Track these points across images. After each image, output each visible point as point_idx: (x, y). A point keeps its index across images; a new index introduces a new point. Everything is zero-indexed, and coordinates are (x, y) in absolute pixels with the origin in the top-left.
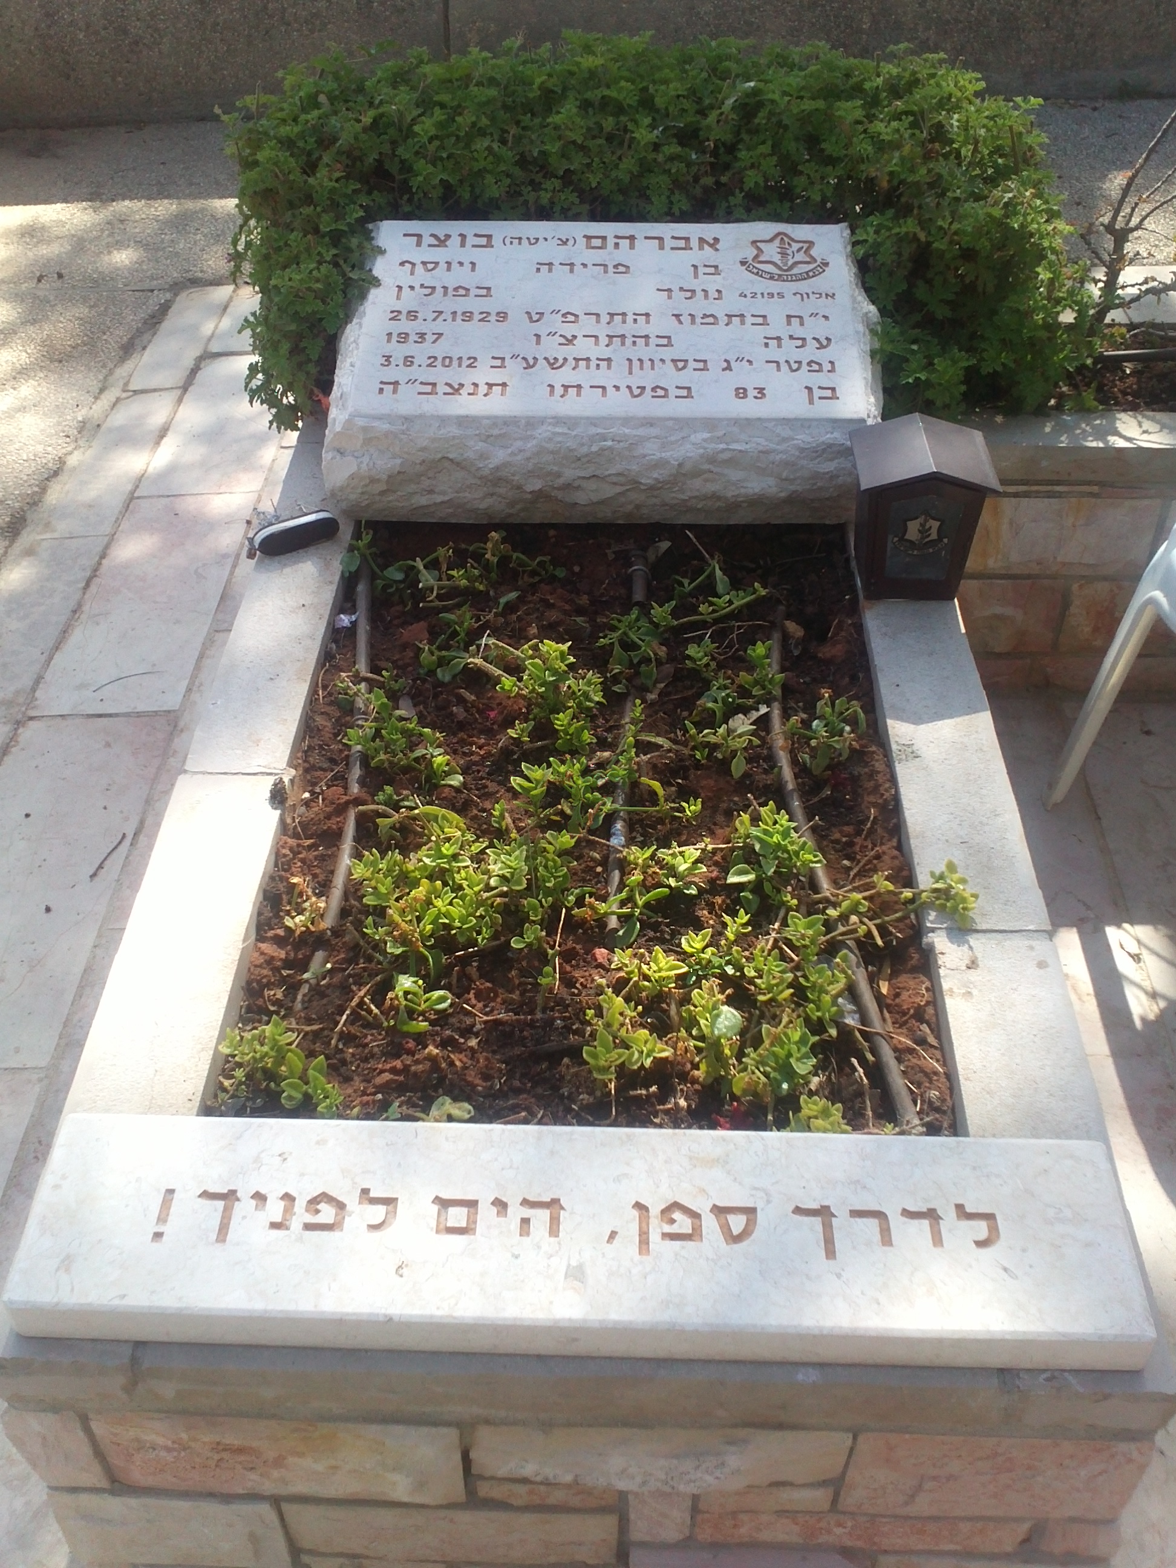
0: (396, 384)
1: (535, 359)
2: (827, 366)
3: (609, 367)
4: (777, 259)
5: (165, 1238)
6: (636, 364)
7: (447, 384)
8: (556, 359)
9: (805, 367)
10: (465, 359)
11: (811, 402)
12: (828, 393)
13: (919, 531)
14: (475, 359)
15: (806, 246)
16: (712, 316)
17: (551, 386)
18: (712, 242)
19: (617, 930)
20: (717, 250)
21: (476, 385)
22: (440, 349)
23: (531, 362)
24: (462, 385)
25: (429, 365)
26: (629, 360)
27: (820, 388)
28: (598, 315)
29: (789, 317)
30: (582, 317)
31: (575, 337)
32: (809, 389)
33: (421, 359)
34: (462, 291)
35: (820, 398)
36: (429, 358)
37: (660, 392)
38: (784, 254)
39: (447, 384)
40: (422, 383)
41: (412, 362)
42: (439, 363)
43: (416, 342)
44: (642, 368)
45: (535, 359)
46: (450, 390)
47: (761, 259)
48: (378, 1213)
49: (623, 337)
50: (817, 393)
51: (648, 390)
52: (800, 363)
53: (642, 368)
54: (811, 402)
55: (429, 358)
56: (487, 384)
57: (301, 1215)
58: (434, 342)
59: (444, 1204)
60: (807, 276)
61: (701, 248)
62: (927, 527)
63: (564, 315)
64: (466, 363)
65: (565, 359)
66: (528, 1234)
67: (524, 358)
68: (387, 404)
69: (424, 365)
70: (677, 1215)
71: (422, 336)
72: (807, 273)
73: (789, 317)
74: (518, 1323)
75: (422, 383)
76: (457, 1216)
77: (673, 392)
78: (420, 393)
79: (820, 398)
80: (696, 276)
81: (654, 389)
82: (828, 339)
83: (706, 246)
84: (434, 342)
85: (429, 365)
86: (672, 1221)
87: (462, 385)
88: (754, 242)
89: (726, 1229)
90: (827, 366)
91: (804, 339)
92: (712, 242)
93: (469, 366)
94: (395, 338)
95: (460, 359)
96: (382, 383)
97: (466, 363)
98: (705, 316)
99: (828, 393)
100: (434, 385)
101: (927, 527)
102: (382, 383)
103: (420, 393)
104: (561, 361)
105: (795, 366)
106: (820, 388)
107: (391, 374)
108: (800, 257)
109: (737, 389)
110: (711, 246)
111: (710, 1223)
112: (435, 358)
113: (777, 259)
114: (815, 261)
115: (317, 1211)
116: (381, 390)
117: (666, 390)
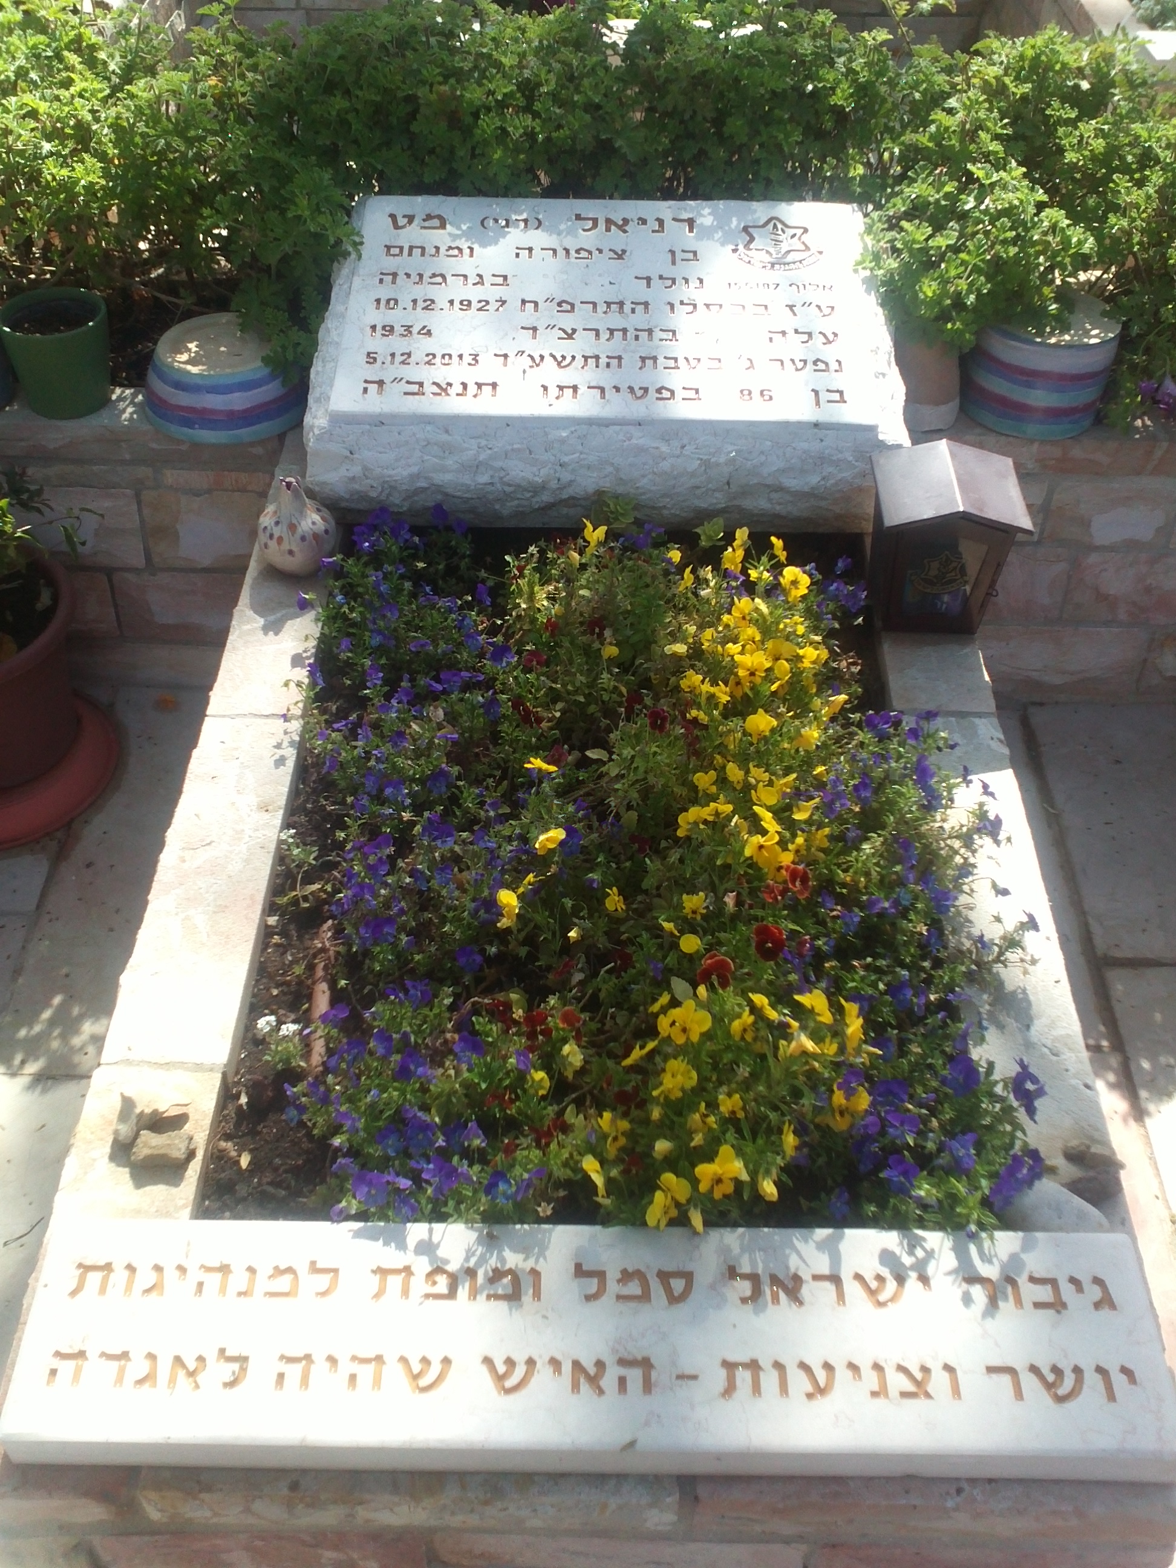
0: (381, 383)
3: (620, 366)
8: (510, 1363)
9: (810, 366)
12: (837, 397)
15: (799, 232)
18: (620, 223)
23: (538, 360)
25: (429, 363)
28: (595, 304)
30: (578, 305)
37: (821, 366)
40: (408, 382)
41: (375, 359)
46: (437, 390)
48: (324, 1280)
49: (625, 331)
50: (824, 396)
52: (805, 362)
57: (263, 1284)
61: (608, 230)
63: (559, 304)
65: (573, 357)
66: (993, 1317)
68: (374, 404)
71: (408, 329)
73: (524, 302)
75: (408, 382)
77: (429, 388)
78: (406, 394)
80: (674, 263)
81: (815, 363)
82: (836, 335)
83: (613, 227)
87: (450, 385)
89: (668, 1290)
90: (834, 366)
91: (810, 334)
93: (403, 363)
96: (366, 381)
97: (399, 359)
99: (837, 397)
100: (421, 384)
102: (366, 381)
103: (406, 394)
104: (568, 359)
107: (373, 373)
110: (620, 227)
111: (655, 1286)
112: (434, 356)
114: (807, 248)
115: (435, 1283)
116: (365, 390)
117: (827, 364)
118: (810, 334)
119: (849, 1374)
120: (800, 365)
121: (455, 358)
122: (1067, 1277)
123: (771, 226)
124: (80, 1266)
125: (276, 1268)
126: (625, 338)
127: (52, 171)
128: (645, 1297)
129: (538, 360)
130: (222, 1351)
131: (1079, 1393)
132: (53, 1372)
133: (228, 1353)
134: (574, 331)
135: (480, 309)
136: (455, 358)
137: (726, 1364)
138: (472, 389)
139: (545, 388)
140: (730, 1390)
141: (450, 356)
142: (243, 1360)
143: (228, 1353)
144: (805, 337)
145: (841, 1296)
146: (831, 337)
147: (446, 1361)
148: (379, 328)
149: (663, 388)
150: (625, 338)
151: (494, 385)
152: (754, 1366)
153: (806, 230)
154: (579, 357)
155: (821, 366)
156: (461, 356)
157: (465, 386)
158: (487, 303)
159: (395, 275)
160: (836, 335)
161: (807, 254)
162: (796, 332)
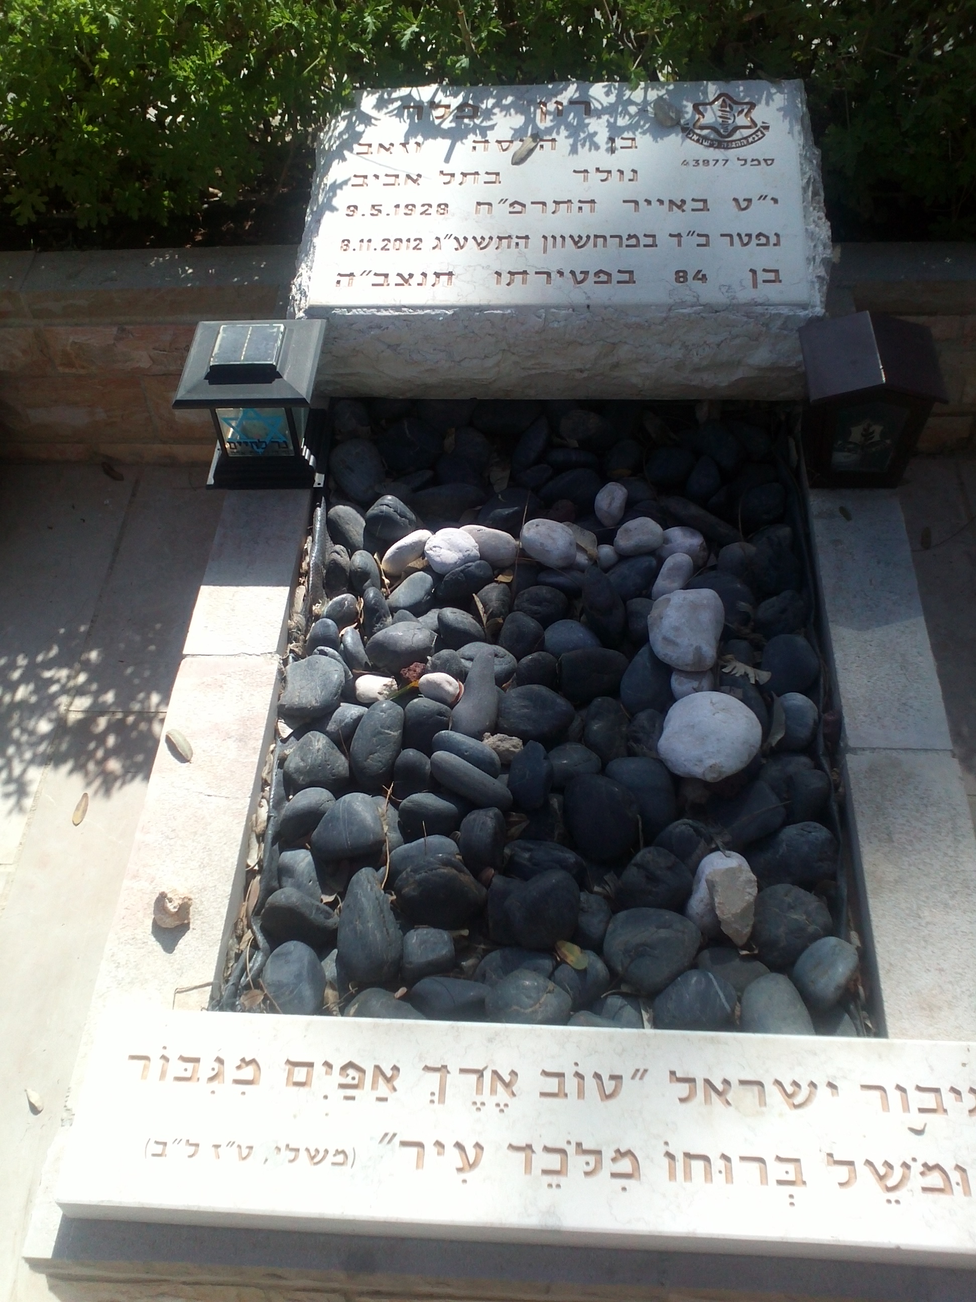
1: (466, 239)
2: (773, 240)
6: (559, 240)
7: (399, 275)
8: (580, 237)
10: (412, 240)
11: (755, 285)
13: (863, 435)
14: (420, 240)
16: (757, 160)
18: (679, 203)
19: (27, 101)
20: (683, 211)
24: (411, 276)
25: (382, 249)
26: (545, 237)
27: (764, 270)
29: (479, 204)
32: (753, 272)
35: (764, 281)
36: (384, 240)
37: (603, 278)
39: (399, 275)
40: (376, 274)
44: (554, 245)
45: (466, 239)
50: (762, 276)
51: (591, 275)
53: (554, 245)
54: (755, 285)
55: (384, 240)
57: (230, 1072)
58: (714, 165)
60: (746, 141)
62: (871, 430)
63: (512, 205)
64: (413, 244)
65: (491, 238)
67: (456, 238)
69: (379, 249)
72: (746, 138)
74: (690, 1235)
75: (376, 274)
77: (616, 277)
79: (764, 281)
81: (597, 274)
83: (674, 207)
84: (714, 165)
87: (411, 276)
90: (773, 240)
92: (679, 203)
95: (408, 240)
98: (753, 160)
100: (386, 276)
101: (871, 430)
102: (340, 275)
104: (584, 239)
109: (677, 272)
110: (679, 207)
117: (767, 238)
120: (580, 277)
122: (914, 1087)
124: (288, 1062)
127: (400, 23)
128: (560, 1094)
130: (288, 1146)
133: (190, 1142)
139: (498, 274)
142: (197, 1145)
143: (190, 1142)
145: (763, 1102)
147: (251, 1148)
151: (450, 274)
155: (763, 240)
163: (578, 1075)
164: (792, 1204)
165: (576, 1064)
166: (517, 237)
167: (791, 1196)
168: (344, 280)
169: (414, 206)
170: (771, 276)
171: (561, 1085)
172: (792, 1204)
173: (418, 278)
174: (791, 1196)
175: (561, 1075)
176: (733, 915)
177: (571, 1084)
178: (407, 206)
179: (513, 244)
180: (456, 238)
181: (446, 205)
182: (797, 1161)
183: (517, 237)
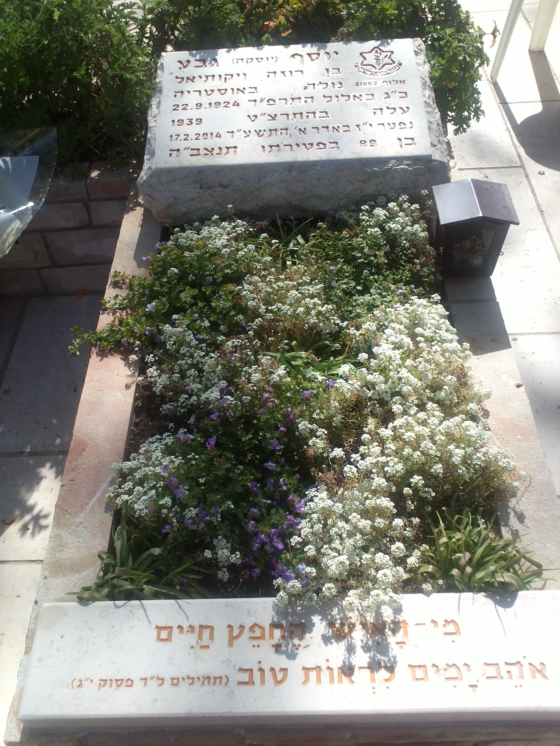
4: (374, 62)
5: (511, 680)
7: (205, 149)
8: (260, 131)
14: (188, 135)
15: (389, 54)
17: (263, 147)
21: (220, 148)
22: (201, 129)
24: (213, 149)
25: (196, 139)
27: (405, 138)
31: (276, 115)
32: (400, 139)
33: (192, 136)
34: (222, 91)
38: (377, 59)
39: (205, 149)
42: (201, 137)
43: (188, 124)
45: (250, 131)
47: (364, 63)
54: (401, 146)
56: (226, 147)
59: (159, 628)
67: (244, 131)
70: (256, 629)
75: (192, 149)
76: (164, 634)
77: (202, 152)
78: (191, 155)
82: (408, 108)
85: (196, 139)
86: (254, 632)
87: (213, 149)
88: (361, 54)
91: (394, 109)
94: (235, 90)
96: (171, 150)
97: (174, 137)
100: (198, 150)
102: (171, 150)
103: (191, 155)
105: (392, 126)
106: (405, 138)
108: (387, 60)
112: (199, 134)
113: (374, 62)
114: (394, 62)
117: (405, 124)
118: (394, 109)
119: (178, 630)
121: (209, 135)
123: (374, 51)
125: (446, 621)
126: (302, 118)
129: (248, 133)
131: (393, 679)
132: (478, 681)
134: (276, 115)
135: (226, 106)
136: (209, 135)
137: (304, 668)
138: (224, 151)
139: (263, 147)
140: (306, 680)
141: (207, 134)
144: (392, 111)
146: (406, 109)
148: (176, 121)
149: (320, 143)
150: (302, 118)
151: (235, 147)
152: (318, 668)
153: (392, 52)
154: (267, 131)
155: (403, 126)
156: (212, 134)
157: (220, 148)
158: (178, 106)
159: (182, 92)
160: (408, 108)
161: (394, 65)
162: (388, 108)
163: (329, 668)
164: (374, 693)
165: (328, 660)
166: (281, 129)
167: (374, 688)
168: (174, 153)
169: (183, 120)
170: (410, 141)
171: (251, 677)
172: (374, 693)
173: (217, 151)
174: (374, 688)
175: (251, 670)
176: (128, 469)
177: (257, 675)
178: (178, 121)
179: (279, 133)
180: (244, 131)
181: (201, 119)
182: (497, 664)
183: (281, 129)
